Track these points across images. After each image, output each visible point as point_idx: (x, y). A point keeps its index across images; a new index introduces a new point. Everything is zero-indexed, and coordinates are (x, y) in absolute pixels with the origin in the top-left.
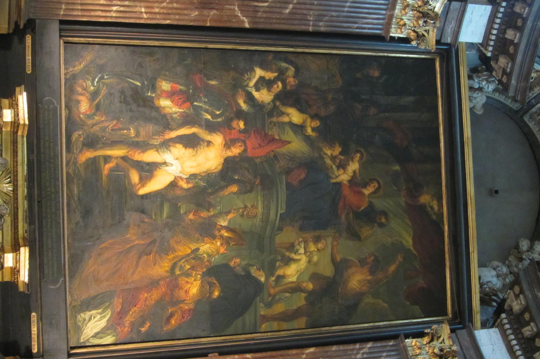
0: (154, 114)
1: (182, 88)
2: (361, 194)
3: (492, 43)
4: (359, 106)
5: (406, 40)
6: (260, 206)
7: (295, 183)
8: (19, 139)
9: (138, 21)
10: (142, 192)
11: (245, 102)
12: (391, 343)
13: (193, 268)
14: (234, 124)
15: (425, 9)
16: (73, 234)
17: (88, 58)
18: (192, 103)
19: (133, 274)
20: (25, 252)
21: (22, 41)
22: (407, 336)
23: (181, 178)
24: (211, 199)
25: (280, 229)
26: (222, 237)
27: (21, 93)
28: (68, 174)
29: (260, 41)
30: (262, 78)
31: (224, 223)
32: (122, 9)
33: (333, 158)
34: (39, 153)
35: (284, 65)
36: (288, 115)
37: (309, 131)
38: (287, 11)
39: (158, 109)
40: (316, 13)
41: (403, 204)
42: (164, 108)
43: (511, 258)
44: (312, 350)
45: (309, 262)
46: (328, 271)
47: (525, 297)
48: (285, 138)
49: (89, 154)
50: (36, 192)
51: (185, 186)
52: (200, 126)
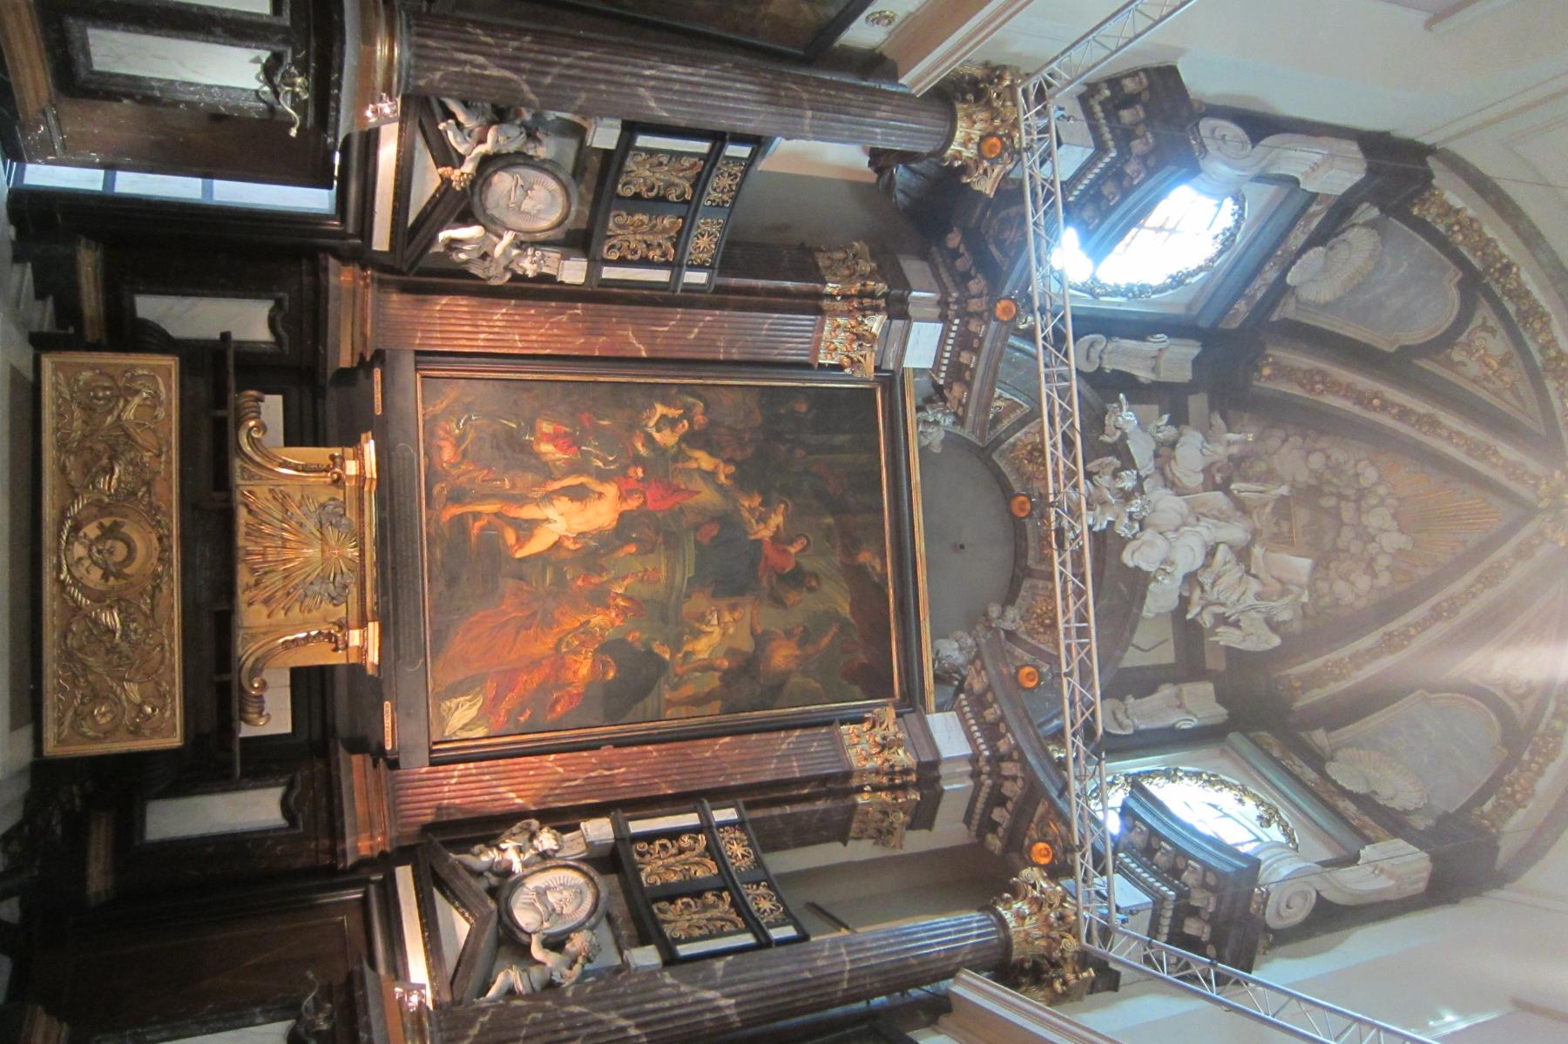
0: (533, 461)
1: (567, 429)
2: (785, 551)
3: (944, 368)
4: (783, 448)
5: (839, 367)
6: (663, 568)
7: (706, 541)
8: (366, 496)
9: (511, 351)
10: (518, 555)
11: (643, 445)
12: (824, 731)
13: (582, 644)
14: (631, 472)
15: (860, 330)
16: (436, 608)
17: (452, 396)
18: (579, 448)
19: (509, 653)
20: (373, 629)
21: (370, 376)
22: (843, 723)
23: (567, 538)
24: (603, 561)
25: (688, 596)
26: (617, 606)
27: (367, 441)
28: (428, 533)
29: (662, 373)
30: (663, 416)
31: (620, 591)
32: (491, 337)
33: (751, 510)
34: (392, 512)
35: (691, 400)
36: (696, 459)
37: (722, 478)
38: (692, 336)
39: (538, 455)
40: (728, 338)
41: (838, 564)
42: (545, 454)
43: (979, 628)
44: (727, 739)
45: (724, 634)
46: (747, 645)
47: (987, 674)
48: (692, 487)
49: (456, 510)
50: (389, 557)
51: (572, 547)
52: (589, 475)
